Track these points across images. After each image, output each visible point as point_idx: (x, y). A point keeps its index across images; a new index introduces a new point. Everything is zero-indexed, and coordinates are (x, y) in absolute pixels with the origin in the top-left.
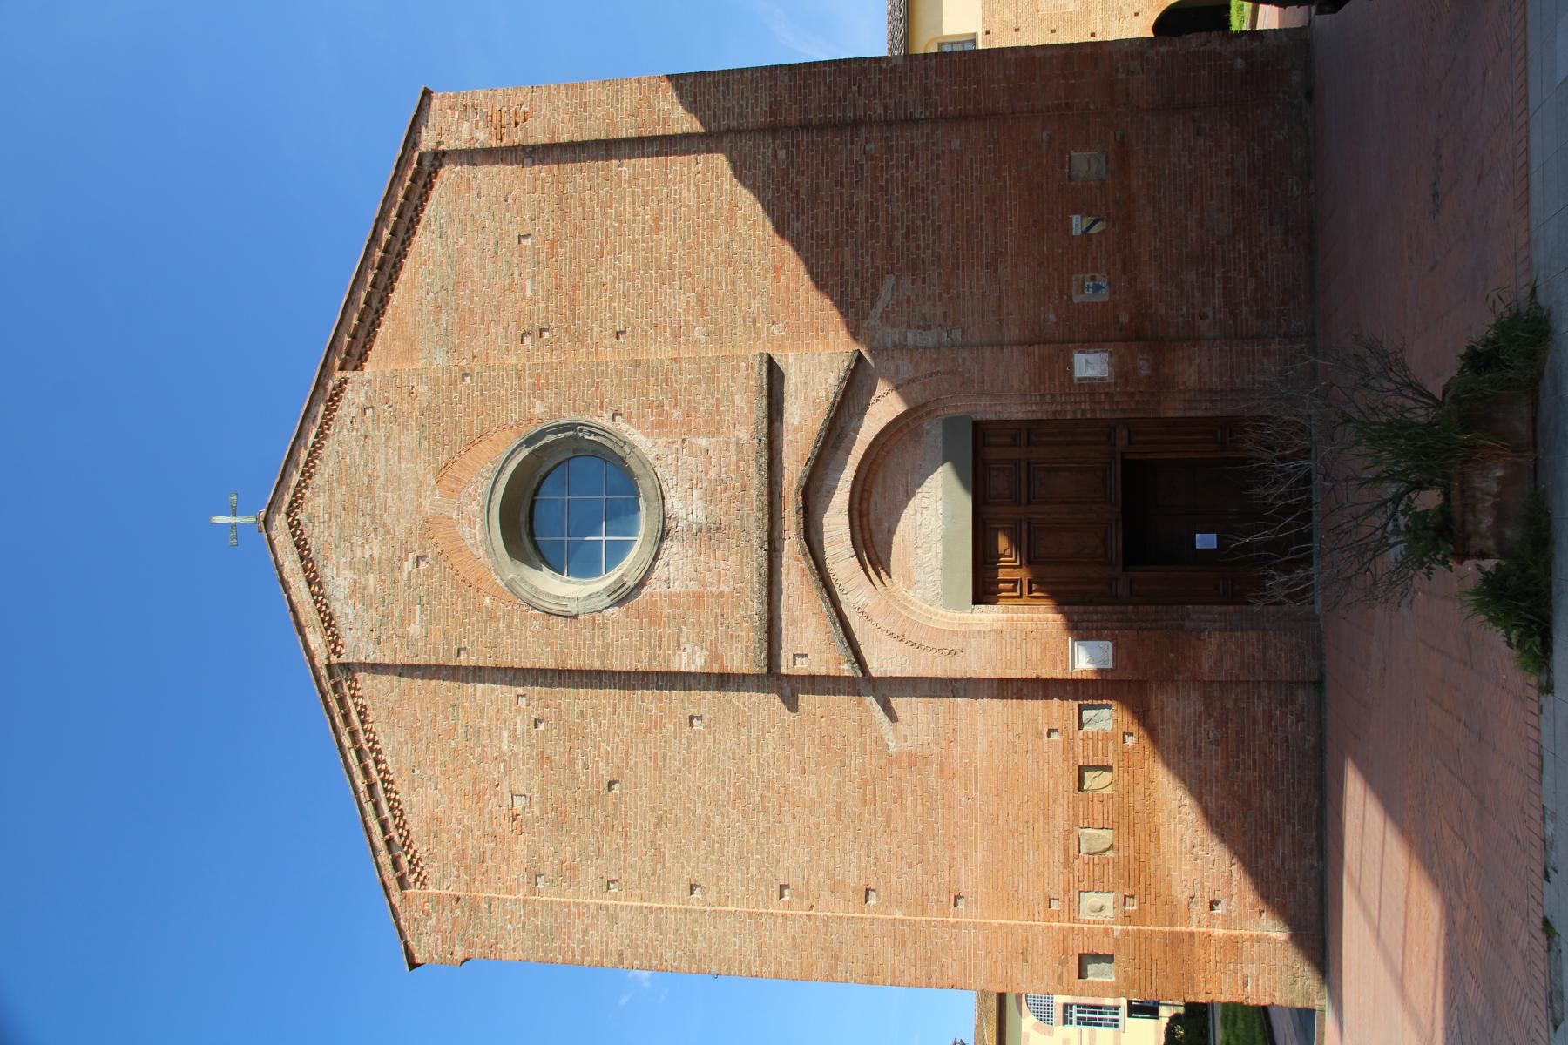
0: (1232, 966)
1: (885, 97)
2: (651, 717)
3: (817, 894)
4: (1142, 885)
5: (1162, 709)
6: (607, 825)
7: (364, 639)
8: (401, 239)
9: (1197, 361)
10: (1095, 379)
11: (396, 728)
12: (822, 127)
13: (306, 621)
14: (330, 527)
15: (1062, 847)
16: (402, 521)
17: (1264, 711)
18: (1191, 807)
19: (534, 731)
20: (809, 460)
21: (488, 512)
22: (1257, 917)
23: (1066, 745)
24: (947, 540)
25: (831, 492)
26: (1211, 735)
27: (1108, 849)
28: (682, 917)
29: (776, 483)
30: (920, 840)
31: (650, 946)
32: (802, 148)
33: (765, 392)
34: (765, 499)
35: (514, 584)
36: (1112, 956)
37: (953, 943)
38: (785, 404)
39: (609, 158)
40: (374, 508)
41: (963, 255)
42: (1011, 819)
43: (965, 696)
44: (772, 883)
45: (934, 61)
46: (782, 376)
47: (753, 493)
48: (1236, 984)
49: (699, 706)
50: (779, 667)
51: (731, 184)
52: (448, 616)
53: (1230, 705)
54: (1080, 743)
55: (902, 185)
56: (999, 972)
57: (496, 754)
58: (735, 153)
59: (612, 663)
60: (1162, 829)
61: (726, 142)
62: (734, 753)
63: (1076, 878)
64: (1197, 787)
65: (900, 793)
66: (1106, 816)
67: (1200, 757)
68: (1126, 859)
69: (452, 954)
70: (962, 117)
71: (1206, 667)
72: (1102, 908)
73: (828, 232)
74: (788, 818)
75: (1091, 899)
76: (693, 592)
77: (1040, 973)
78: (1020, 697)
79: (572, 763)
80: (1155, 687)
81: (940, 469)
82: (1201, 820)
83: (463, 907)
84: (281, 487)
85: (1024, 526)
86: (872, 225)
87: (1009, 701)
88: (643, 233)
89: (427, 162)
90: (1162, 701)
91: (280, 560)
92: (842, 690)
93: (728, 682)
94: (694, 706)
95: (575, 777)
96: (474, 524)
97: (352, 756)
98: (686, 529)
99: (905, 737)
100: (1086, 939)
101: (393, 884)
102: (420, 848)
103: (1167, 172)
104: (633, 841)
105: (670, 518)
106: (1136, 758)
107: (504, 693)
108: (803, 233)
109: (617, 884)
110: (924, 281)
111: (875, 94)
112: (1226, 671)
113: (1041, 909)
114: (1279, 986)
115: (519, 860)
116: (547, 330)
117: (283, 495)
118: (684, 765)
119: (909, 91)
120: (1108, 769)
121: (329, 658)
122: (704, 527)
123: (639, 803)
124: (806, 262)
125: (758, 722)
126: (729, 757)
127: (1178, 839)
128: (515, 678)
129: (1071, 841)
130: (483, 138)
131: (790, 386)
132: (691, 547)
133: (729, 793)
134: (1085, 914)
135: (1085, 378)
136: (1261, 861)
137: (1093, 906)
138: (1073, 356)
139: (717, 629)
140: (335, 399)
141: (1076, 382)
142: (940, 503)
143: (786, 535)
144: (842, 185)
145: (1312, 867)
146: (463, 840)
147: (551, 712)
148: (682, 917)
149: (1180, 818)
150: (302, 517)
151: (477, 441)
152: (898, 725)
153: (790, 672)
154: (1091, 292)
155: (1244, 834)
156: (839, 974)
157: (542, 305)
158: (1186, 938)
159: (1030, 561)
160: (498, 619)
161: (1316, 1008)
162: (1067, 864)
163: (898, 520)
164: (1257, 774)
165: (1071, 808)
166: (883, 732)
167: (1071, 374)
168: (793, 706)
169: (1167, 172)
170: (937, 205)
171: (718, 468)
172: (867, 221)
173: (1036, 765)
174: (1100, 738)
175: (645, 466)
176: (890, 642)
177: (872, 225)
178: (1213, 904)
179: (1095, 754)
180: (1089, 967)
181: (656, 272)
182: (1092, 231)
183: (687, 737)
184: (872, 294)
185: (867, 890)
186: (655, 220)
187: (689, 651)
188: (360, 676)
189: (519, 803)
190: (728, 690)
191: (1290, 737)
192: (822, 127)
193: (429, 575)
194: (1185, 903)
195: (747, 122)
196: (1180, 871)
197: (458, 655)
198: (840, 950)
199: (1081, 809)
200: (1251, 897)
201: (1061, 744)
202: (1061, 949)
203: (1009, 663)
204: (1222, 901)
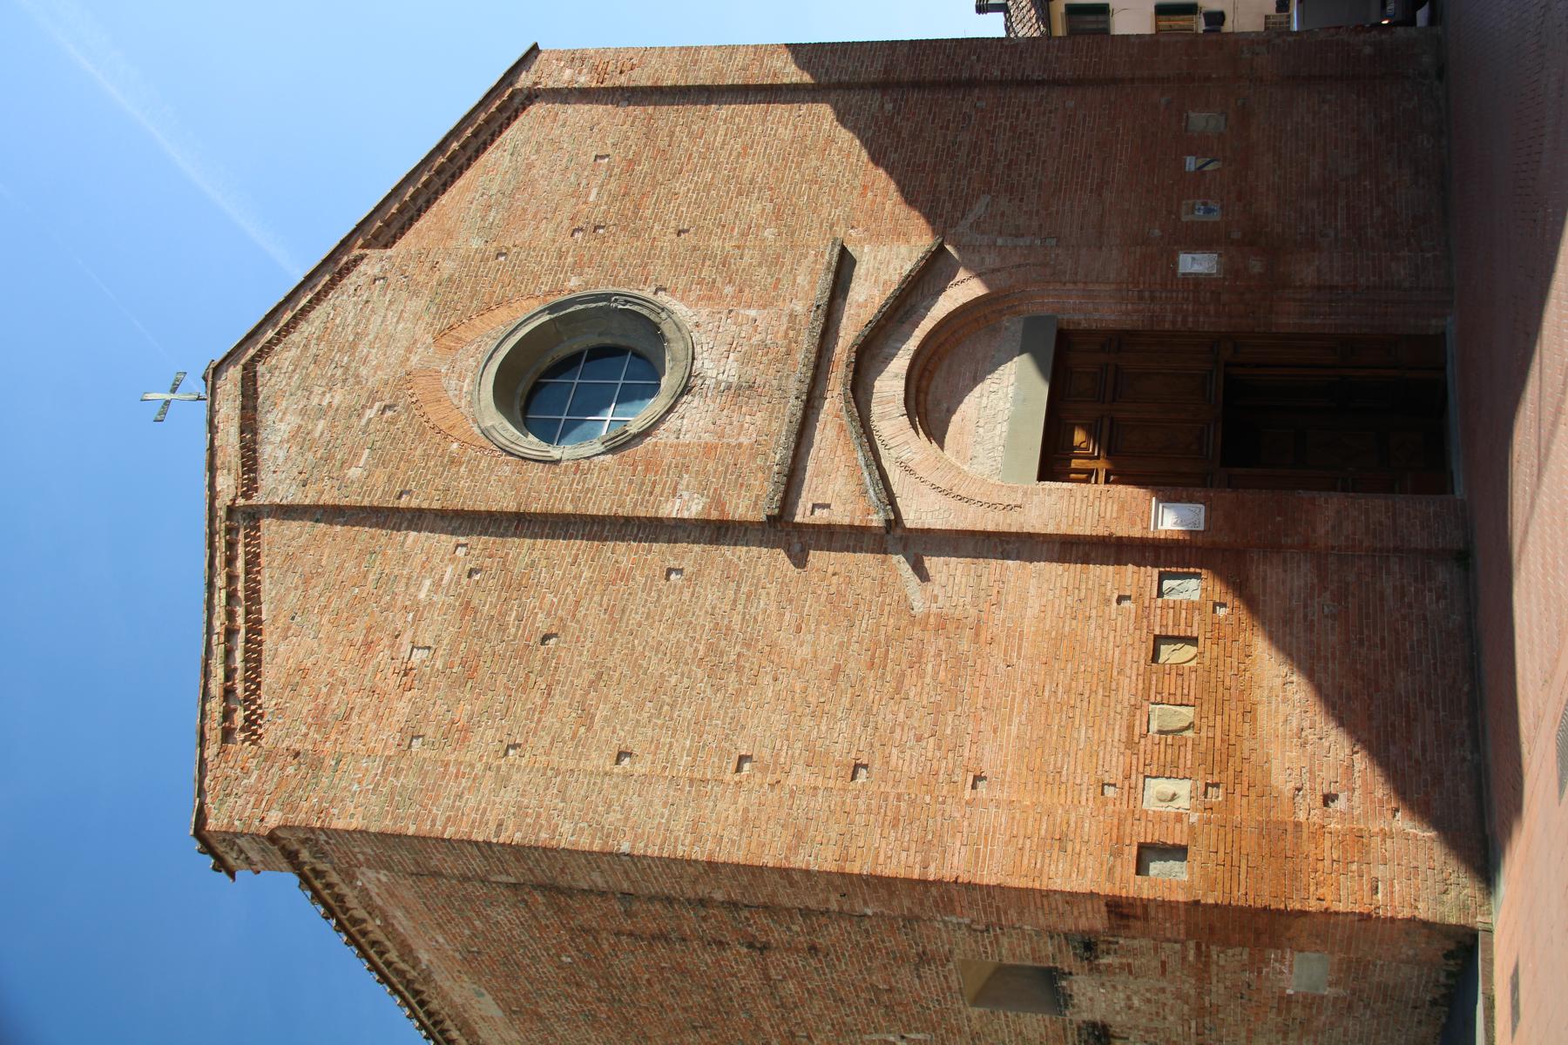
0: (1354, 867)
1: (1004, 64)
2: (618, 569)
3: (787, 769)
4: (1231, 772)
5: (1264, 580)
6: (526, 682)
7: (288, 481)
8: (468, 154)
9: (1317, 263)
10: (1201, 274)
11: (289, 573)
12: (935, 85)
13: (223, 463)
14: (290, 378)
15: (1125, 723)
16: (379, 373)
17: (1395, 588)
18: (1299, 685)
19: (465, 581)
20: (870, 322)
21: (485, 366)
22: (1390, 817)
23: (1140, 612)
24: (1013, 420)
25: (888, 359)
26: (1326, 609)
27: (1187, 728)
28: (599, 781)
29: (827, 350)
30: (937, 709)
31: (544, 816)
32: (910, 103)
33: (833, 269)
34: (813, 357)
35: (493, 431)
36: (1196, 639)
37: (966, 823)
38: (852, 285)
39: (709, 102)
40: (349, 362)
41: (1067, 182)
42: (1060, 689)
43: (1018, 558)
44: (729, 753)
45: (1057, 42)
46: (853, 262)
47: (800, 357)
48: (1362, 889)
49: (683, 558)
50: (794, 516)
51: (831, 125)
52: (401, 459)
53: (1351, 578)
54: (1158, 611)
55: (1010, 130)
56: (1025, 861)
57: (408, 603)
58: (840, 104)
59: (587, 506)
60: (1259, 707)
61: (833, 96)
62: (714, 608)
63: (1142, 760)
64: (1306, 660)
65: (920, 656)
66: (1186, 691)
67: (1312, 631)
68: (1211, 741)
69: (262, 820)
70: (1078, 82)
71: (1321, 531)
72: (1174, 797)
73: (925, 163)
74: (769, 678)
75: (1159, 786)
76: (706, 443)
77: (1082, 865)
78: (1086, 561)
79: (503, 614)
80: (1255, 558)
81: (1015, 359)
82: (1312, 699)
83: (300, 764)
84: (249, 342)
85: (1106, 423)
86: (973, 159)
87: (1072, 566)
88: (729, 156)
89: (517, 101)
90: (1265, 571)
91: (217, 407)
92: (865, 548)
93: (725, 535)
94: (676, 559)
95: (503, 628)
96: (465, 378)
97: (220, 598)
98: (712, 387)
99: (936, 597)
100: (1150, 825)
101: (214, 735)
102: (266, 701)
103: (1289, 128)
104: (556, 699)
105: (696, 376)
106: (1229, 630)
108: (898, 162)
109: (519, 750)
110: (1021, 200)
111: (993, 62)
112: (1347, 537)
113: (1091, 795)
114: (1424, 895)
115: (395, 719)
116: (603, 227)
117: (248, 349)
118: (647, 619)
119: (1028, 60)
120: (1193, 641)
121: (234, 500)
122: (734, 385)
123: (576, 658)
124: (898, 183)
125: (753, 577)
126: (707, 612)
127: (1281, 719)
128: (460, 527)
129: (1138, 716)
130: (584, 80)
131: (860, 271)
132: (714, 402)
133: (696, 651)
134: (1151, 803)
135: (1191, 274)
137: (1163, 793)
138: (1178, 256)
139: (725, 478)
140: (348, 269)
141: (1179, 276)
142: (1011, 389)
143: (829, 395)
144: (948, 129)
145: (1464, 759)
146: (329, 694)
147: (493, 562)
148: (599, 781)
149: (1285, 697)
150: (261, 368)
151: (494, 307)
152: (929, 586)
153: (807, 520)
154: (1202, 213)
155: (1370, 717)
156: (800, 858)
157: (604, 207)
158: (1290, 828)
159: (1111, 452)
160: (461, 464)
161: (1480, 926)
162: (1130, 744)
163: (960, 402)
164: (1385, 652)
165: (1140, 682)
166: (909, 591)
167: (1175, 271)
168: (800, 561)
169: (1289, 128)
170: (1044, 145)
171: (764, 335)
172: (968, 156)
173: (1099, 632)
174: (1184, 606)
175: (680, 330)
176: (933, 496)
177: (973, 159)
178: (1328, 799)
179: (1176, 624)
180: (1152, 865)
181: (735, 186)
182: (1206, 169)
183: (660, 591)
184: (965, 208)
185: (857, 767)
186: (744, 149)
187: (686, 495)
188: (268, 526)
189: (419, 655)
190: (723, 544)
191: (1429, 615)
192: (935, 85)
193: (393, 422)
194: (1291, 795)
195: (859, 78)
196: (1283, 758)
197: (400, 497)
198: (806, 828)
199: (1154, 682)
200: (1381, 791)
201: (1133, 611)
202: (1114, 837)
203: (1077, 520)
204: (1341, 796)
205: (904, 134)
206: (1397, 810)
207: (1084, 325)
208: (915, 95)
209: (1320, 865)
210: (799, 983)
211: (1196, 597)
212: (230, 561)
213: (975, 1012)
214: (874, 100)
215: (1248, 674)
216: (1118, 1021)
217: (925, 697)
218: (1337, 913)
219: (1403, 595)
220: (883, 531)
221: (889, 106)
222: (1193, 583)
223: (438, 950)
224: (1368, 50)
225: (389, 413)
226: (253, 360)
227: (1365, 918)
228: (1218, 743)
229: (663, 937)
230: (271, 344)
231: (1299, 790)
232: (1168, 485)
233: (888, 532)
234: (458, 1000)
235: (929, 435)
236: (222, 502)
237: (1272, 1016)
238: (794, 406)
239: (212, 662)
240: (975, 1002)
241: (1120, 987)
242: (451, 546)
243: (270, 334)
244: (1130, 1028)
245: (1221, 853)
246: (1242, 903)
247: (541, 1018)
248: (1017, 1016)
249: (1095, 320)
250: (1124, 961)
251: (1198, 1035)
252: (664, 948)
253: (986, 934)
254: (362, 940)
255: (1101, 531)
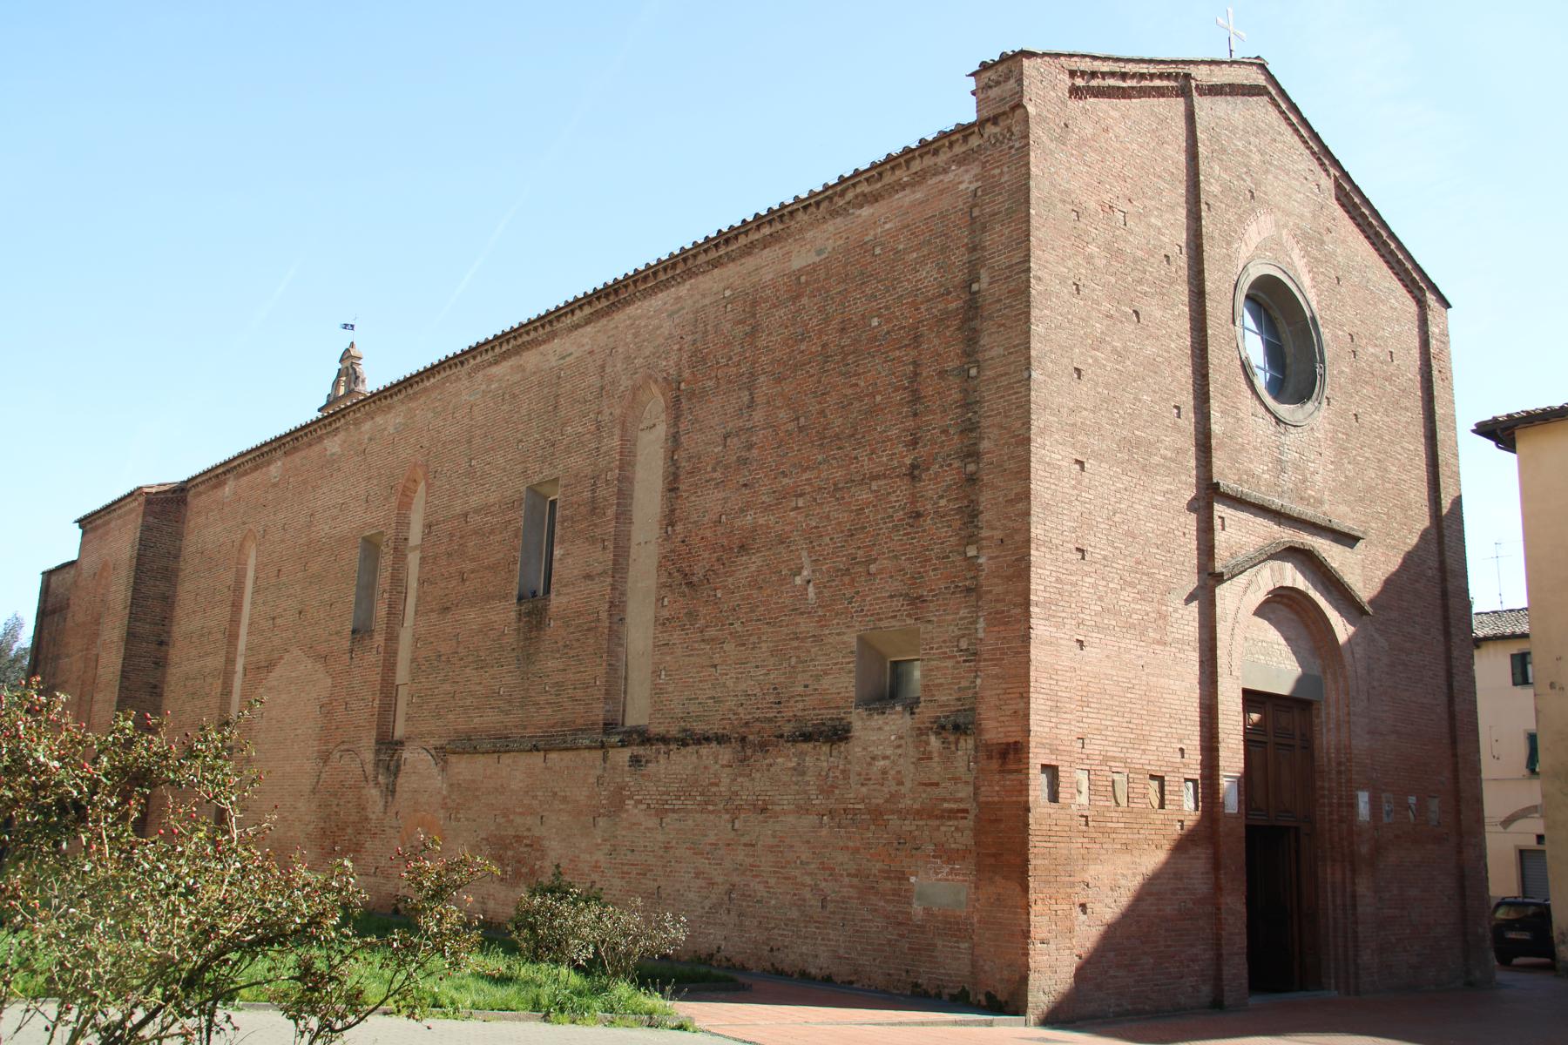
4: (1095, 835)
27: (1116, 802)
39: (1426, 437)
46: (1352, 547)
50: (1217, 502)
61: (1434, 531)
78: (1202, 724)
97: (1143, 69)
107: (1182, 237)
120: (1162, 806)
136: (1112, 954)
145: (1110, 1006)
150: (1266, 98)
197: (1207, 204)
204: (1086, 916)
205: (1417, 585)
206: (1080, 958)
207: (1317, 721)
208: (1437, 592)
209: (1053, 901)
210: (871, 502)
211: (1186, 808)
212: (1161, 76)
213: (851, 639)
214: (1433, 562)
215: (1146, 846)
216: (856, 749)
217: (1123, 603)
218: (1028, 914)
219: (1192, 961)
220: (1211, 571)
221: (1430, 573)
222: (1192, 805)
223: (875, 223)
224: (1480, 930)
225: (1249, 195)
226: (1269, 94)
227: (1026, 934)
228: (1110, 825)
229: (916, 397)
230: (1278, 106)
231: (1087, 886)
232: (1247, 781)
233: (1210, 574)
234: (809, 235)
235: (1266, 602)
236: (1192, 70)
237: (879, 865)
238: (1277, 502)
239: (1110, 63)
240: (861, 639)
241: (899, 751)
242: (1180, 243)
243: (1284, 106)
244: (846, 758)
245: (1057, 828)
246: (1031, 844)
247: (795, 298)
248: (850, 672)
249: (1321, 729)
250: (935, 754)
251: (845, 810)
252: (901, 399)
253: (955, 649)
254: (888, 167)
255: (1221, 736)
